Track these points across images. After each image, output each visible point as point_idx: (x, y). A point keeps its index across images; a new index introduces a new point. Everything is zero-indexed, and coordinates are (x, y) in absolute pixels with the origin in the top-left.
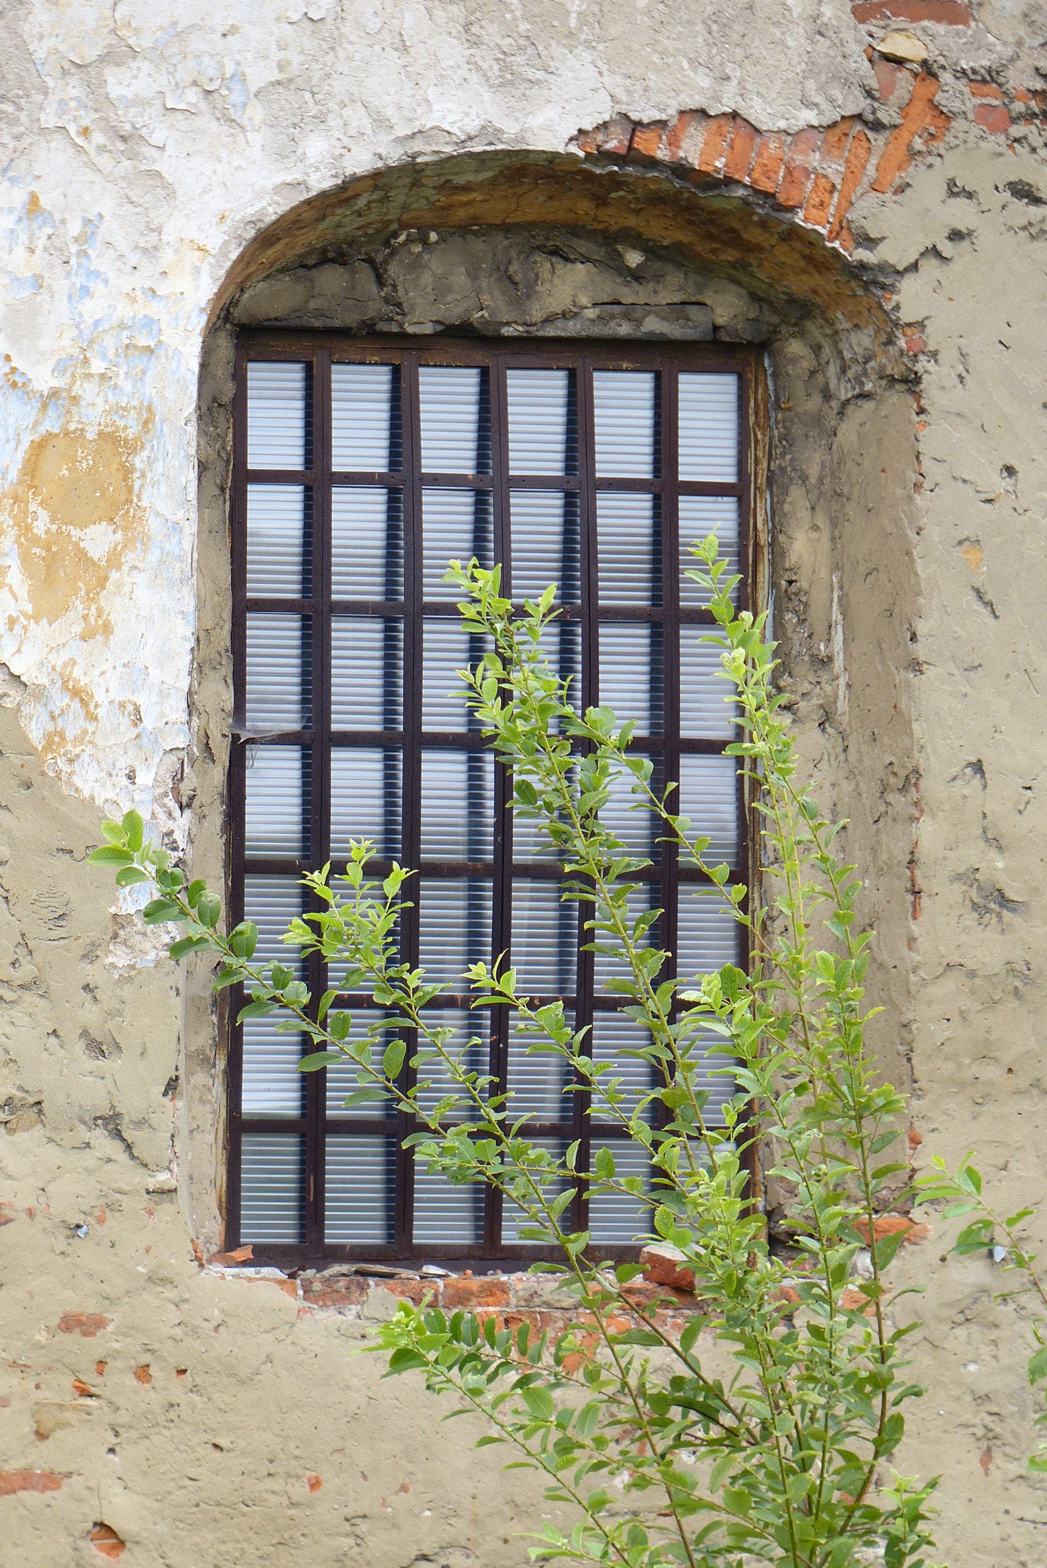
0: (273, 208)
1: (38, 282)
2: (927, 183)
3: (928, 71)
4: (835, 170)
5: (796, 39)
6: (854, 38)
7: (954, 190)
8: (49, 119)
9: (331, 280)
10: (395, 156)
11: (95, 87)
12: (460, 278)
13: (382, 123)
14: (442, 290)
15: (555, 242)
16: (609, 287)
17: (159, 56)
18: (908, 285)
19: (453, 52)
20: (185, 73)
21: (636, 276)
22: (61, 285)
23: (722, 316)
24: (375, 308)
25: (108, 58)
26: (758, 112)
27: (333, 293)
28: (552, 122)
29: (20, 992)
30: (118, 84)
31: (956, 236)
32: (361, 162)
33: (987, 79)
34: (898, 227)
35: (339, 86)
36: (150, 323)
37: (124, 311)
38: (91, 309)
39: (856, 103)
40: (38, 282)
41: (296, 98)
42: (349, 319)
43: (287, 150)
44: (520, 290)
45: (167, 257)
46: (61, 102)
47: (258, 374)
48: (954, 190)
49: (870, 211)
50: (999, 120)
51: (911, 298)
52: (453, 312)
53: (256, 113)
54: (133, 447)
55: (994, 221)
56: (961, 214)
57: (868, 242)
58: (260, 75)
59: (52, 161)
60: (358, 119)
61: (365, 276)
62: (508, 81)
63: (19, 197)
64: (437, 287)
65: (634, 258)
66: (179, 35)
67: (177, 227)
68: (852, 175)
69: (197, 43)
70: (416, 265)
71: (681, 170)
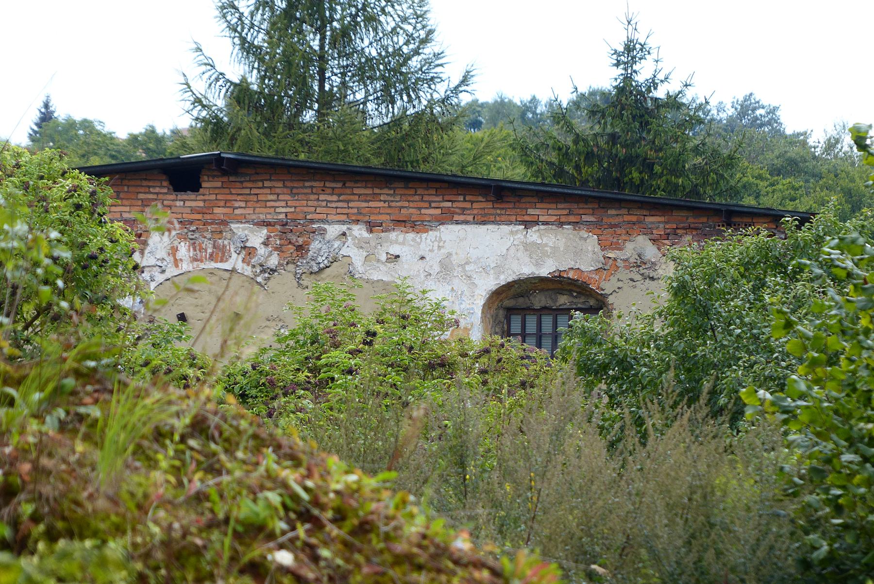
0: (494, 288)
1: (453, 302)
2: (614, 280)
3: (615, 260)
4: (597, 277)
5: (590, 255)
6: (601, 254)
7: (619, 280)
8: (455, 274)
9: (521, 300)
10: (516, 278)
11: (464, 268)
12: (543, 298)
13: (514, 273)
14: (540, 301)
15: (561, 291)
16: (571, 299)
17: (475, 263)
18: (610, 297)
19: (527, 259)
20: (479, 265)
21: (576, 297)
22: (457, 303)
23: (591, 304)
24: (529, 304)
25: (466, 263)
26: (583, 268)
27: (521, 302)
28: (544, 272)
29: (233, 335)
30: (467, 268)
31: (619, 288)
32: (510, 279)
33: (625, 260)
34: (608, 287)
35: (506, 267)
36: (473, 309)
37: (468, 307)
38: (462, 306)
39: (600, 266)
40: (453, 302)
41: (499, 269)
42: (525, 306)
43: (497, 278)
44: (555, 301)
45: (476, 297)
46: (458, 271)
47: (513, 317)
48: (619, 280)
49: (603, 284)
50: (626, 267)
51: (611, 300)
52: (543, 304)
53: (492, 272)
54: (470, 330)
55: (626, 286)
56: (620, 284)
57: (603, 290)
58: (492, 265)
59: (456, 281)
60: (510, 272)
61: (527, 299)
62: (537, 265)
63: (450, 288)
64: (539, 300)
65: (575, 294)
66: (479, 259)
67: (477, 292)
68: (600, 278)
69: (482, 260)
70: (535, 296)
71: (569, 278)
